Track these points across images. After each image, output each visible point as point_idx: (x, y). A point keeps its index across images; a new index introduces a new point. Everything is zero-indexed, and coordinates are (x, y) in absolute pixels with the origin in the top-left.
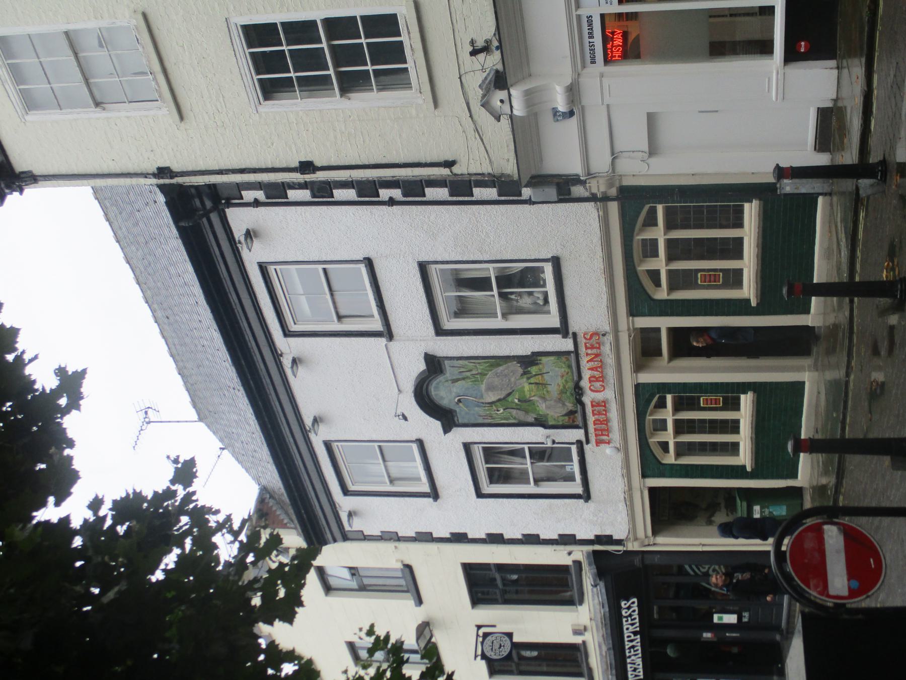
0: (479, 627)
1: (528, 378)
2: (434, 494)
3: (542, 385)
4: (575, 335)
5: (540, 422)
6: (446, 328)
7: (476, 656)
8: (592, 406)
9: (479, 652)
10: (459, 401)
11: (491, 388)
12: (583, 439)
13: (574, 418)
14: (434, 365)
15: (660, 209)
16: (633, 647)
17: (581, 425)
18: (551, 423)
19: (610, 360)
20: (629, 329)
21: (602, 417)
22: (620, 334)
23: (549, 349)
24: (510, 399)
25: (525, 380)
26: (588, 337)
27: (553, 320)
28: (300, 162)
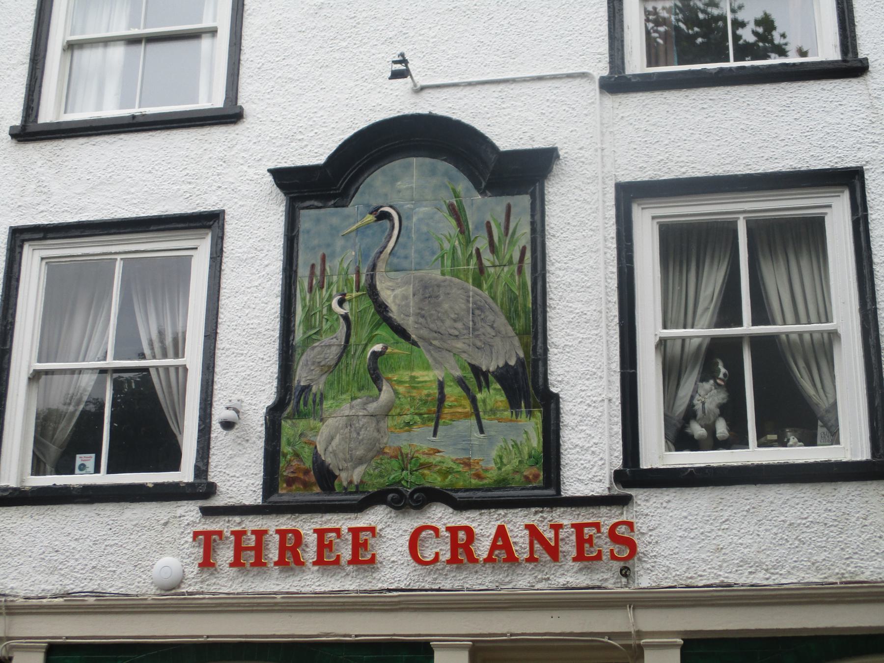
1: (461, 382)
2: (28, 132)
3: (436, 410)
4: (623, 501)
5: (290, 400)
6: (27, 249)
8: (355, 532)
10: (386, 216)
11: (428, 293)
12: (218, 501)
13: (299, 483)
14: (525, 173)
17: (274, 498)
18: (287, 428)
19: (523, 581)
20: (640, 634)
21: (310, 554)
22: (630, 613)
23: (571, 438)
25: (458, 373)
26: (622, 530)
27: (655, 454)
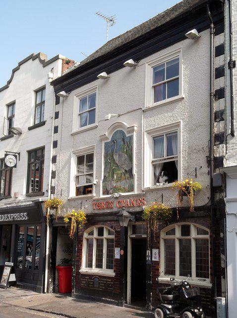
0: (19, 154)
7: (7, 152)
9: (8, 153)
15: (207, 236)
16: (8, 217)
24: (115, 165)
28: (87, 216)
